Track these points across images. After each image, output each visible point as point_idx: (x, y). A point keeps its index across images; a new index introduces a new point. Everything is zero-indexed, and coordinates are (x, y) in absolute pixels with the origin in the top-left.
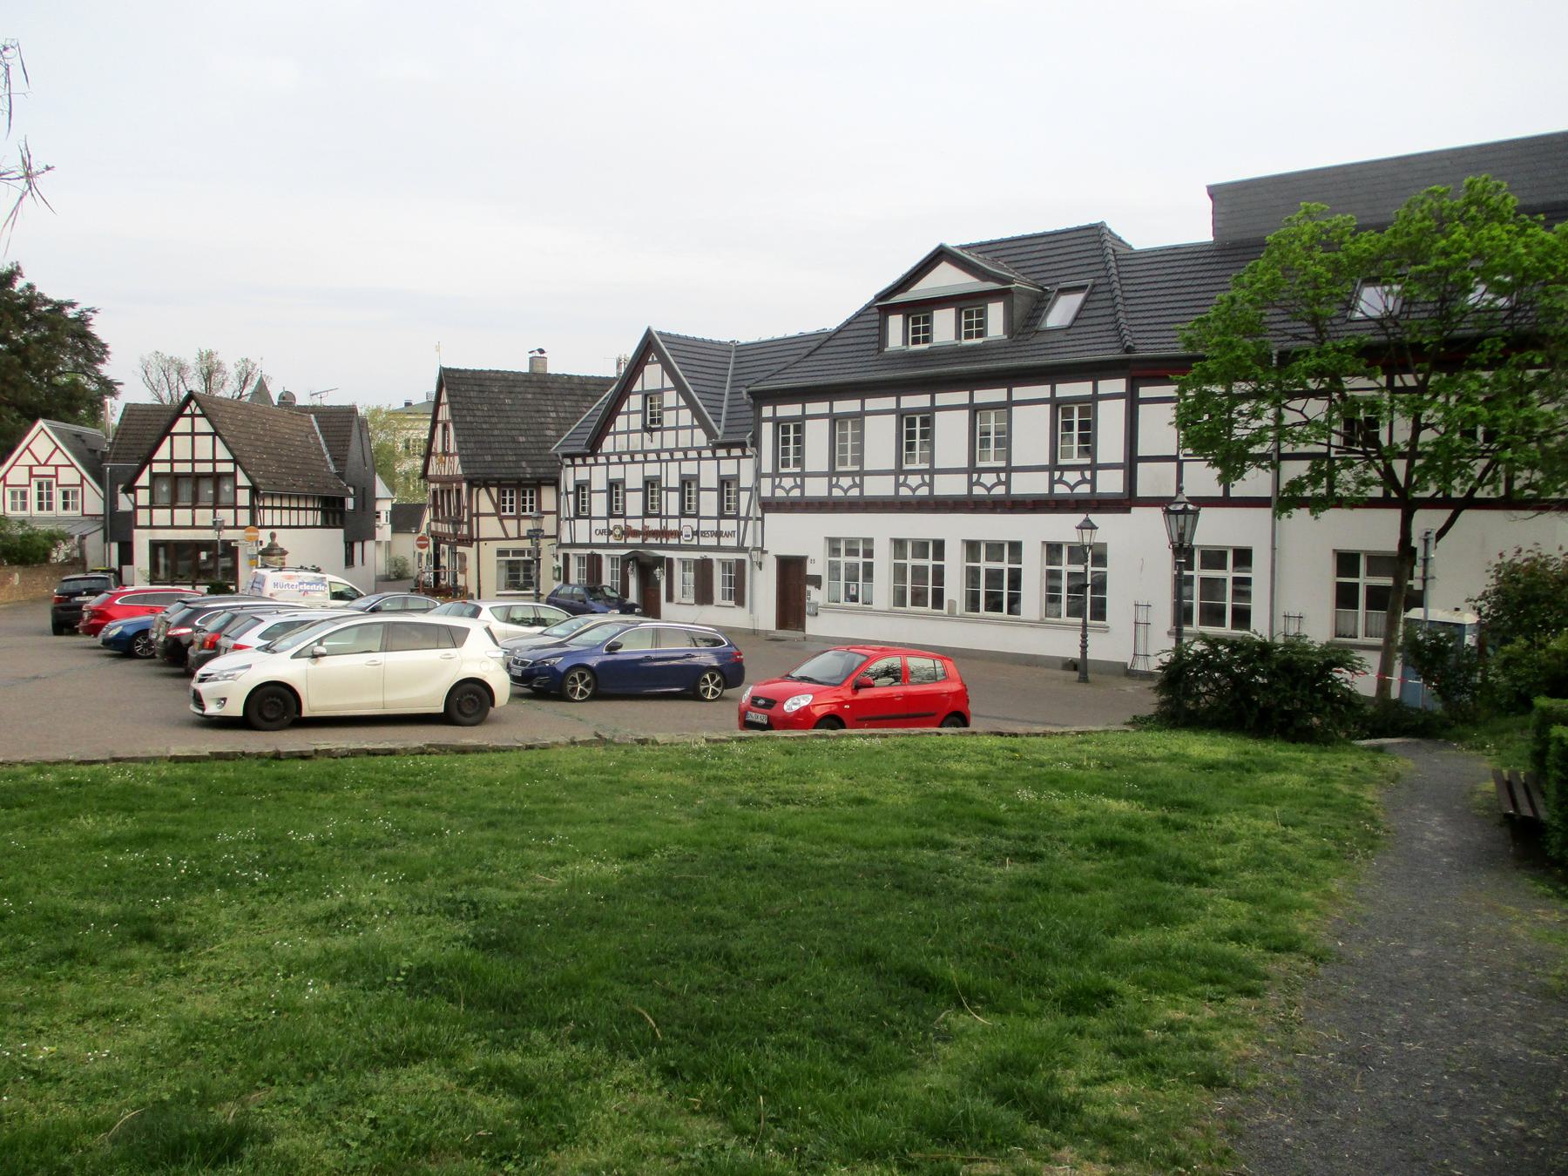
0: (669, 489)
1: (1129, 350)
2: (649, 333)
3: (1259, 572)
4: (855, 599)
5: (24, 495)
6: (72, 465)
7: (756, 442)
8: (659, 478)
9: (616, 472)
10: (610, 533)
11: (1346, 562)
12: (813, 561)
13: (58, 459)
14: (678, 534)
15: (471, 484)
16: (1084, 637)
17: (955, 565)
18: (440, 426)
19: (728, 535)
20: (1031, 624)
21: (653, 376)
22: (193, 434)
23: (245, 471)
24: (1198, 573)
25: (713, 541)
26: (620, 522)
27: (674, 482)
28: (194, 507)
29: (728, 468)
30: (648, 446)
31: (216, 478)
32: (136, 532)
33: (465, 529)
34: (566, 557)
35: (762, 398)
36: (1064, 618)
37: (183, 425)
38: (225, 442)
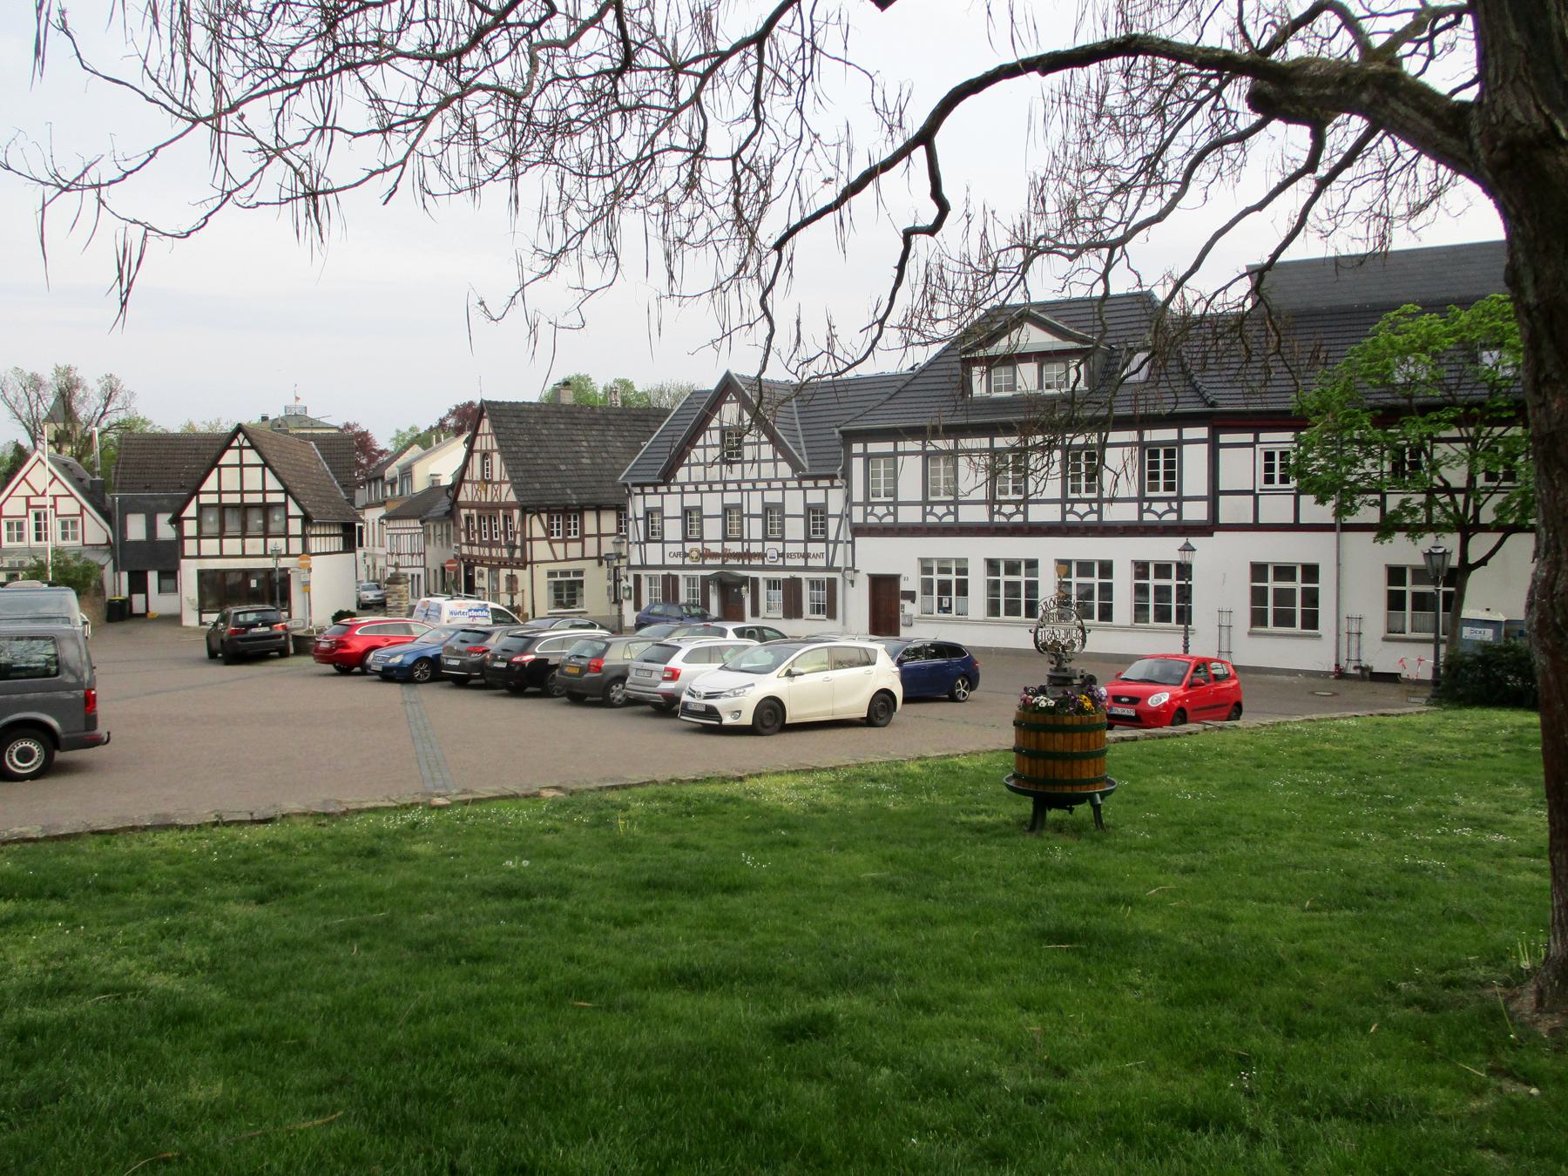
0: (750, 516)
1: (1213, 404)
2: (728, 376)
3: (1325, 586)
4: (948, 610)
5: (20, 526)
6: (72, 495)
7: (847, 475)
8: (740, 507)
9: (692, 500)
10: (685, 555)
11: (1396, 574)
12: (906, 579)
13: (57, 489)
14: (762, 556)
15: (525, 510)
16: (1186, 639)
17: (1123, 584)
18: (477, 457)
19: (816, 556)
20: (1123, 629)
21: (730, 412)
22: (241, 466)
23: (297, 502)
24: (1152, 582)
25: (800, 562)
26: (698, 545)
27: (757, 508)
28: (244, 536)
29: (815, 497)
30: (730, 477)
31: (266, 508)
32: (183, 561)
33: (518, 554)
34: (637, 579)
35: (849, 437)
36: (1271, 628)
37: (230, 457)
38: (275, 473)
